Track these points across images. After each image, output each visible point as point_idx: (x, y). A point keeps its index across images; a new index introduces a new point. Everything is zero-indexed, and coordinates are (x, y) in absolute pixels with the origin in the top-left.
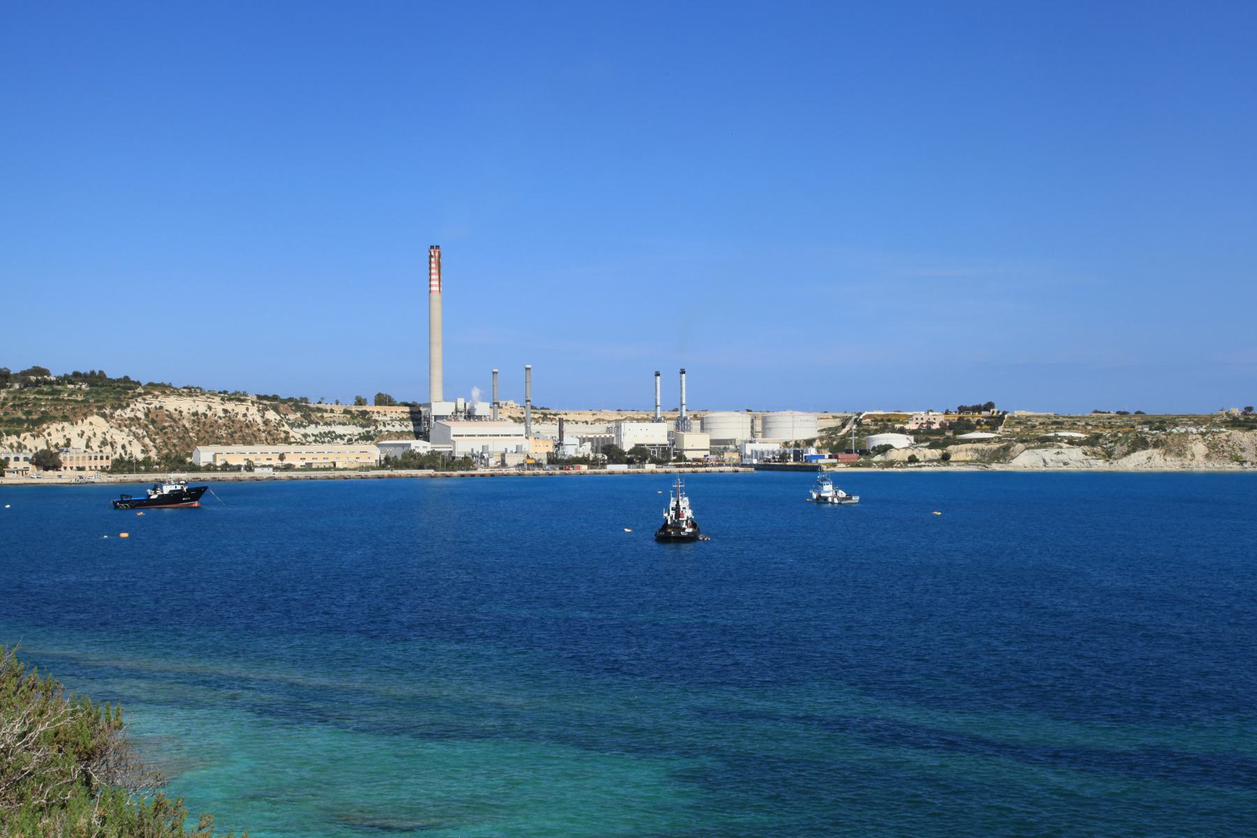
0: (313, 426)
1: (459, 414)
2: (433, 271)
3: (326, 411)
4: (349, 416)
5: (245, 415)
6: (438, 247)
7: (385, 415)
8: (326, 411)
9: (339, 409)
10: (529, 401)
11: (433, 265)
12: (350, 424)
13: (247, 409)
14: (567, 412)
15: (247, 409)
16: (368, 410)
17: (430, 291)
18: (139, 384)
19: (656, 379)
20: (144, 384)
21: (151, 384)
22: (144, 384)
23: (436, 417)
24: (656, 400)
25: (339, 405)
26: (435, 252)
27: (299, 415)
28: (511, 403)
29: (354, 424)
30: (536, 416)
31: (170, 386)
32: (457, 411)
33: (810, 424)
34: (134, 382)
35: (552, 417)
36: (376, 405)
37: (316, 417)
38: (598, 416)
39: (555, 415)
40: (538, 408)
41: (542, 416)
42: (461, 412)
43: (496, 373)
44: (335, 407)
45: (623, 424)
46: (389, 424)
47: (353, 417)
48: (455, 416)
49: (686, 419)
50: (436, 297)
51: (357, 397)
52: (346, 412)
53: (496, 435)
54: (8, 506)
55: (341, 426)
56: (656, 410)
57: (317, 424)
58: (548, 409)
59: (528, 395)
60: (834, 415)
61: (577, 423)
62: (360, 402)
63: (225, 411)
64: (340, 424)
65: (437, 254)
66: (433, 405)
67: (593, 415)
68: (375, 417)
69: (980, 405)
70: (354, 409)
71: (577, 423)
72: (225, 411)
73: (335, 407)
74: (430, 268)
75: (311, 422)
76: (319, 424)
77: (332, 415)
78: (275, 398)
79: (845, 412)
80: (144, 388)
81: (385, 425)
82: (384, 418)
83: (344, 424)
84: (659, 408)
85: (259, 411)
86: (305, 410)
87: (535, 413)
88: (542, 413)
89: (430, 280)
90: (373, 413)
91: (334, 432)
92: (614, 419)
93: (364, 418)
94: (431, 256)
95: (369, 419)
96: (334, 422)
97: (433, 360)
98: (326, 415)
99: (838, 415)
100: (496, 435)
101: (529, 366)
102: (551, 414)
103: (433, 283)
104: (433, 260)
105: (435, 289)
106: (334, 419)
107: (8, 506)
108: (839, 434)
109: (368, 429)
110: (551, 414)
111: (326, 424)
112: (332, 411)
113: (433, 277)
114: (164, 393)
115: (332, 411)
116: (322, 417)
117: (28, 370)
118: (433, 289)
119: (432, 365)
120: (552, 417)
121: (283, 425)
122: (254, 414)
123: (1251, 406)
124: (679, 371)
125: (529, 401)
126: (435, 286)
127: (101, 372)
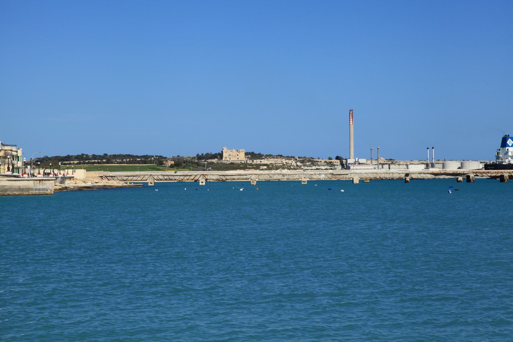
0: (315, 166)
1: (356, 162)
2: (351, 118)
3: (319, 162)
4: (326, 163)
5: (291, 164)
6: (352, 110)
7: (338, 163)
8: (319, 162)
9: (323, 161)
10: (372, 159)
11: (351, 116)
12: (326, 166)
13: (292, 162)
14: (400, 161)
15: (292, 162)
16: (332, 161)
17: (350, 124)
18: (263, 155)
19: (427, 150)
20: (265, 155)
21: (267, 155)
22: (265, 155)
23: (349, 164)
24: (427, 157)
25: (323, 160)
26: (351, 112)
27: (310, 163)
28: (382, 158)
29: (328, 166)
30: (389, 163)
31: (272, 155)
32: (355, 162)
33: (476, 165)
34: (262, 155)
35: (395, 163)
36: (336, 159)
37: (316, 164)
38: (411, 163)
39: (396, 162)
40: (344, 159)
41: (391, 163)
42: (357, 162)
43: (379, 148)
44: (322, 160)
45: (409, 165)
46: (339, 166)
47: (327, 164)
48: (355, 163)
49: (433, 163)
50: (352, 126)
51: (329, 157)
52: (325, 162)
53: (364, 169)
54: (343, 191)
55: (323, 166)
56: (433, 160)
57: (316, 166)
58: (394, 160)
59: (378, 156)
60: (481, 161)
61: (403, 165)
62: (330, 159)
63: (286, 163)
64: (323, 166)
65: (352, 113)
66: (348, 160)
67: (410, 162)
68: (335, 163)
69: (250, 152)
70: (328, 161)
71: (403, 165)
72: (286, 163)
73: (322, 160)
74: (350, 117)
75: (314, 165)
76: (316, 166)
77: (321, 163)
78: (288, 157)
79: (438, 160)
80: (265, 157)
81: (337, 166)
82: (337, 164)
83: (324, 166)
84: (433, 159)
85: (295, 162)
86: (313, 162)
87: (389, 162)
88: (391, 162)
89: (350, 121)
90: (334, 162)
91: (321, 168)
92: (417, 163)
93: (331, 164)
94: (350, 113)
95: (332, 164)
96: (321, 165)
97: (350, 146)
98: (319, 163)
99: (483, 161)
100: (364, 169)
101: (379, 147)
102: (394, 162)
103: (350, 121)
104: (350, 114)
105: (351, 123)
106: (321, 164)
107: (343, 191)
108: (79, 162)
109: (332, 167)
110: (394, 162)
111: (319, 166)
112: (321, 162)
113: (351, 120)
114: (270, 158)
115: (321, 162)
116: (317, 164)
117: (60, 156)
118: (350, 123)
119: (350, 147)
120: (395, 163)
121: (302, 167)
122: (294, 163)
123: (166, 157)
124: (432, 147)
125: (372, 159)
126: (351, 122)
127: (104, 154)
